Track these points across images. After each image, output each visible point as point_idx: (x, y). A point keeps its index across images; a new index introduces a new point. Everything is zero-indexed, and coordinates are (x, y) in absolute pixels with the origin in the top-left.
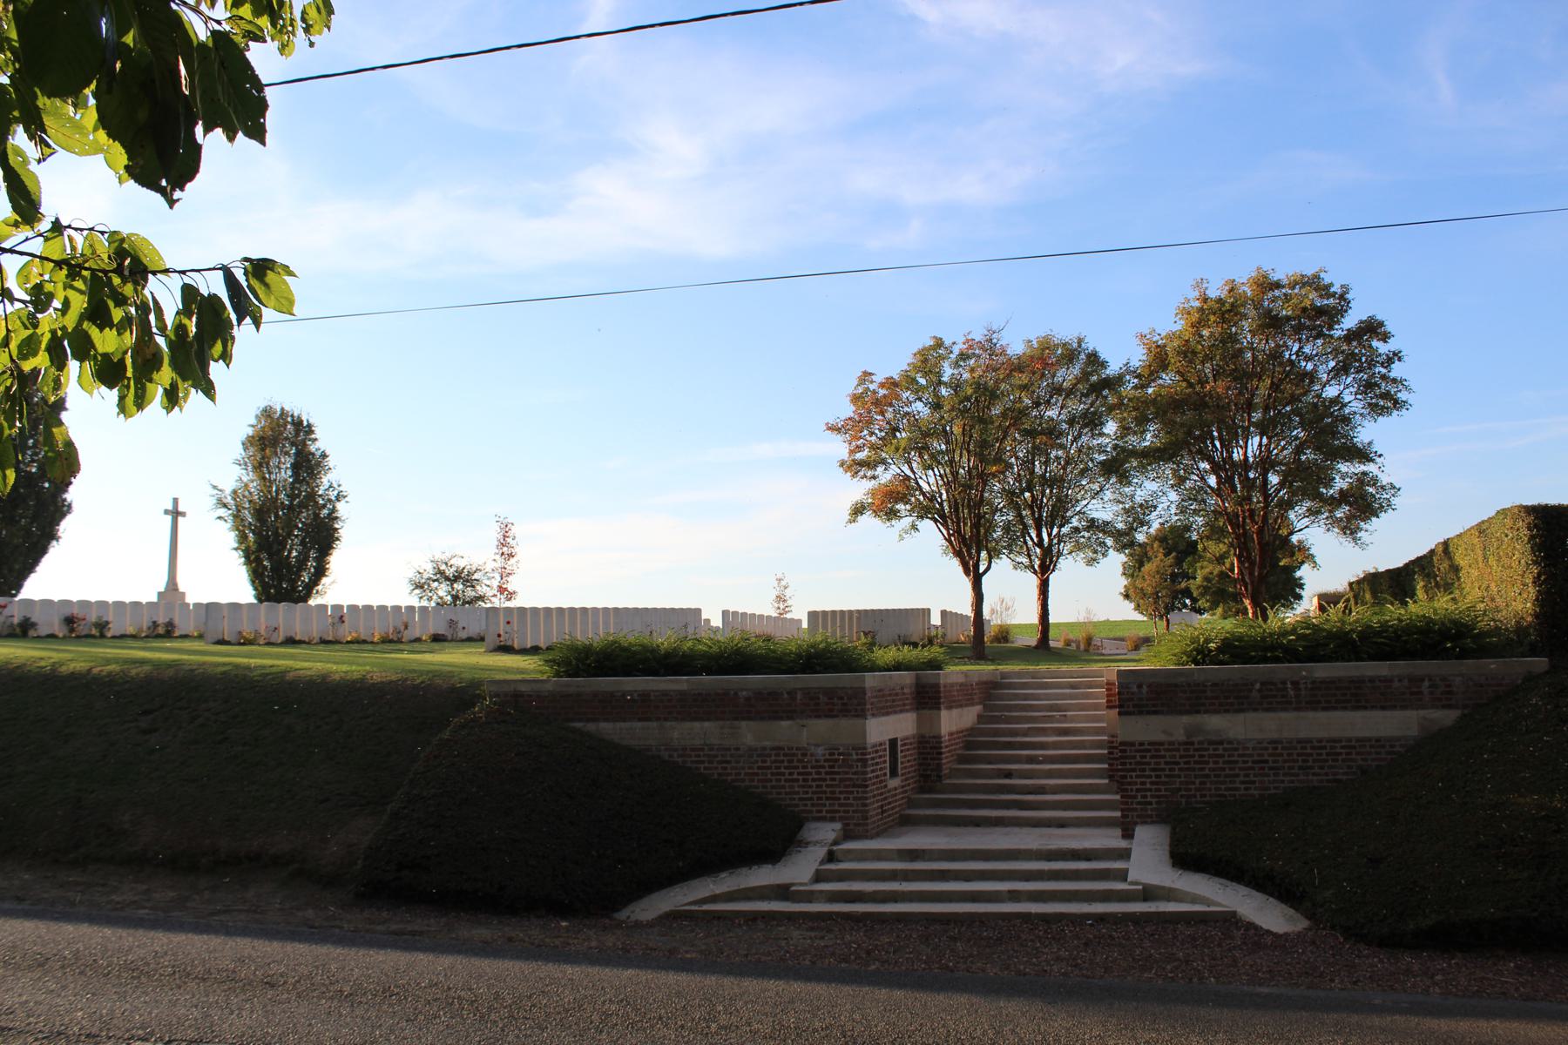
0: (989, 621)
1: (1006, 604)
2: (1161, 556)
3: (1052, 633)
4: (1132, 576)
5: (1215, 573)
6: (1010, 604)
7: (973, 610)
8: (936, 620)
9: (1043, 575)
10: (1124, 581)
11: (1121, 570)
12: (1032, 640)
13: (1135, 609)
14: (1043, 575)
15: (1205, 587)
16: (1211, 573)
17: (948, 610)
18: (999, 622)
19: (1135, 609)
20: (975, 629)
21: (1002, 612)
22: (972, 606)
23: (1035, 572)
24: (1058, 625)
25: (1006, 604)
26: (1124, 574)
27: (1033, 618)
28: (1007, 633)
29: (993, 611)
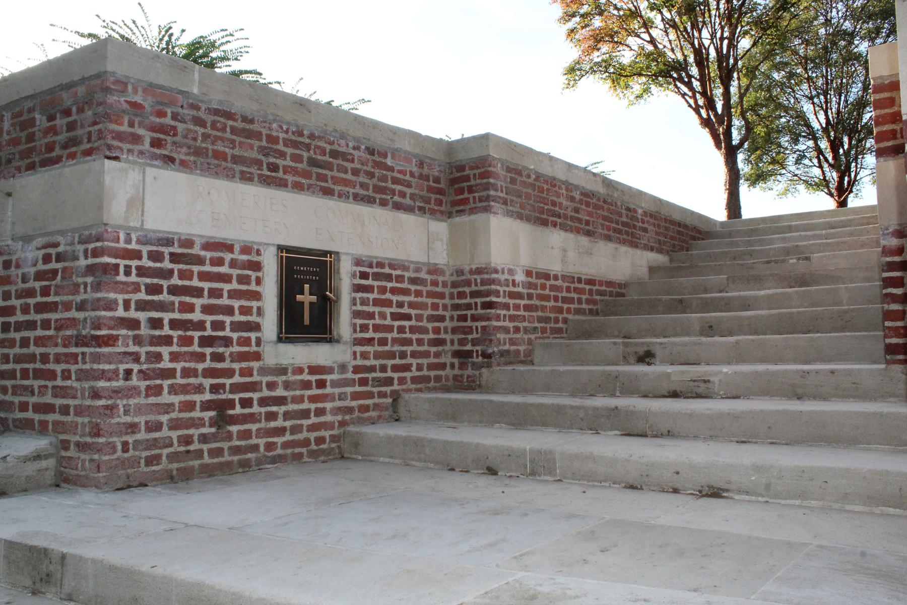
7: (726, 190)
14: (840, 197)
22: (725, 185)
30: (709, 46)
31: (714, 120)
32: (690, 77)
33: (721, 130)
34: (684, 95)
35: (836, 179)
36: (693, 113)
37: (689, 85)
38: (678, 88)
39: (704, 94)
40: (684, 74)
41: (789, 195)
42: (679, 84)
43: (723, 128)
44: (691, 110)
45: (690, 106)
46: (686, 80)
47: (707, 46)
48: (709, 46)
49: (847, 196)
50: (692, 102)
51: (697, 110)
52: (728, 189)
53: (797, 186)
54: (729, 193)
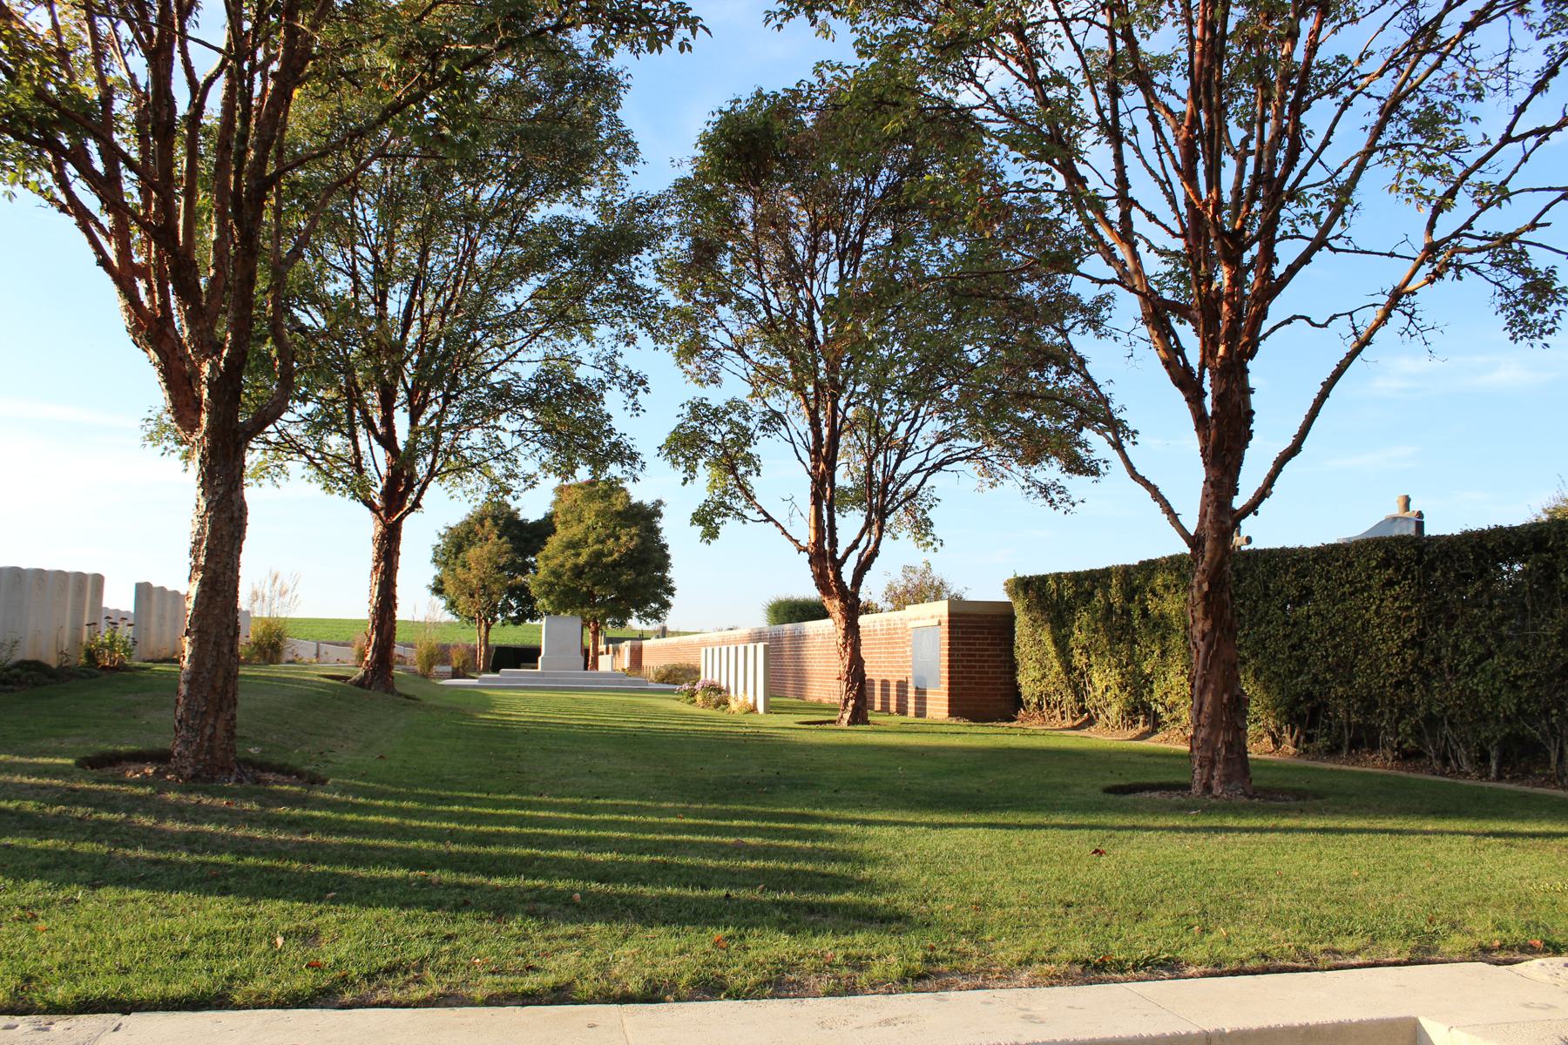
0: (248, 613)
1: (282, 584)
2: (494, 537)
3: (400, 636)
4: (446, 564)
5: (568, 565)
6: (289, 585)
7: (195, 568)
8: (118, 598)
9: (389, 514)
10: (434, 571)
11: (431, 555)
12: (349, 663)
13: (446, 608)
14: (389, 514)
15: (551, 585)
16: (562, 566)
17: (155, 584)
18: (266, 615)
19: (446, 608)
20: (198, 646)
21: (272, 599)
22: (194, 552)
23: (370, 504)
24: (413, 625)
25: (282, 584)
26: (435, 561)
27: (358, 606)
28: (280, 637)
29: (255, 596)
30: (210, 81)
31: (186, 334)
32: (112, 154)
33: (206, 369)
34: (84, 218)
35: (384, 470)
36: (113, 289)
37: (107, 186)
38: (65, 186)
39: (162, 234)
40: (92, 146)
41: (267, 482)
42: (70, 169)
43: (214, 367)
44: (107, 278)
45: (104, 262)
46: (99, 165)
47: (201, 79)
48: (210, 81)
49: (401, 518)
50: (111, 250)
51: (124, 277)
52: (204, 569)
53: (288, 464)
54: (203, 583)
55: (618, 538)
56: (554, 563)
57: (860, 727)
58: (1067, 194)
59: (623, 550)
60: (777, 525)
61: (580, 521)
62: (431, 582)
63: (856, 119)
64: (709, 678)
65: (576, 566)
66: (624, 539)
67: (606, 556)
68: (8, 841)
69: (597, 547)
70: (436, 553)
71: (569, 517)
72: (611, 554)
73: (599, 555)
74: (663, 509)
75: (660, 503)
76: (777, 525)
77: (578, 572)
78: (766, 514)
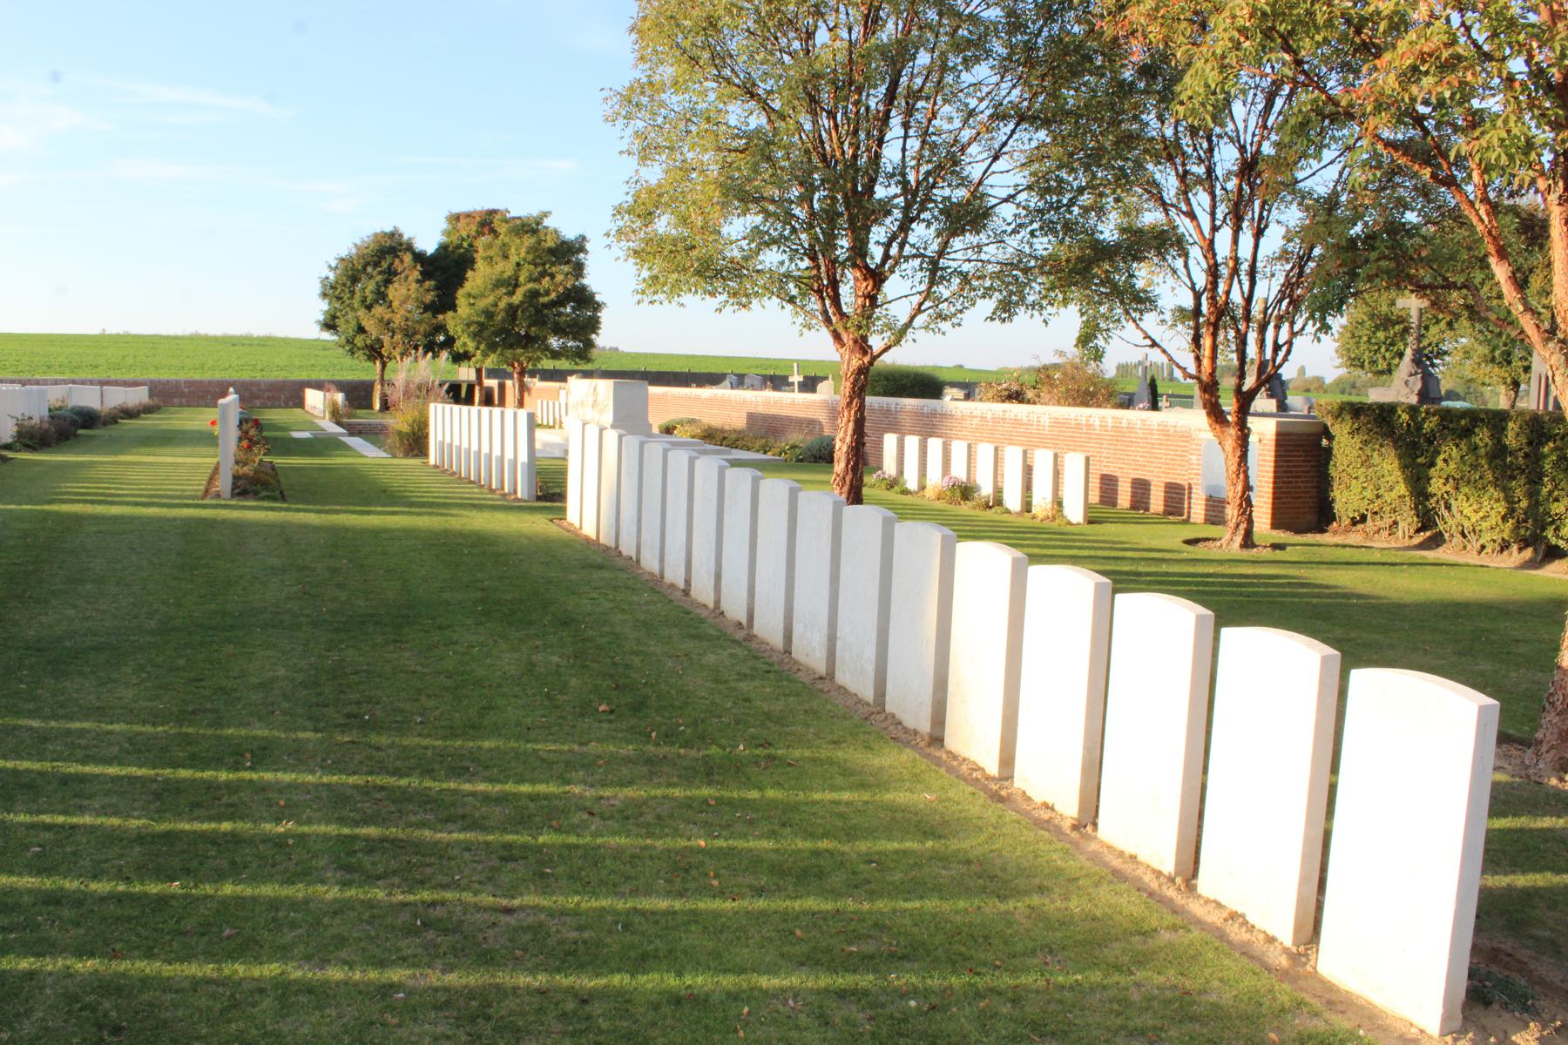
5: (502, 305)
55: (552, 276)
56: (483, 304)
57: (1171, 518)
58: (1345, 78)
59: (561, 289)
60: (1164, 351)
61: (506, 257)
62: (321, 318)
63: (1522, 93)
64: (551, 403)
65: (510, 306)
66: (559, 278)
67: (543, 296)
68: (1561, 822)
69: (530, 285)
70: (324, 286)
71: (491, 253)
72: (547, 293)
73: (534, 294)
74: (588, 246)
75: (584, 238)
76: (1164, 351)
77: (512, 311)
78: (1153, 341)
